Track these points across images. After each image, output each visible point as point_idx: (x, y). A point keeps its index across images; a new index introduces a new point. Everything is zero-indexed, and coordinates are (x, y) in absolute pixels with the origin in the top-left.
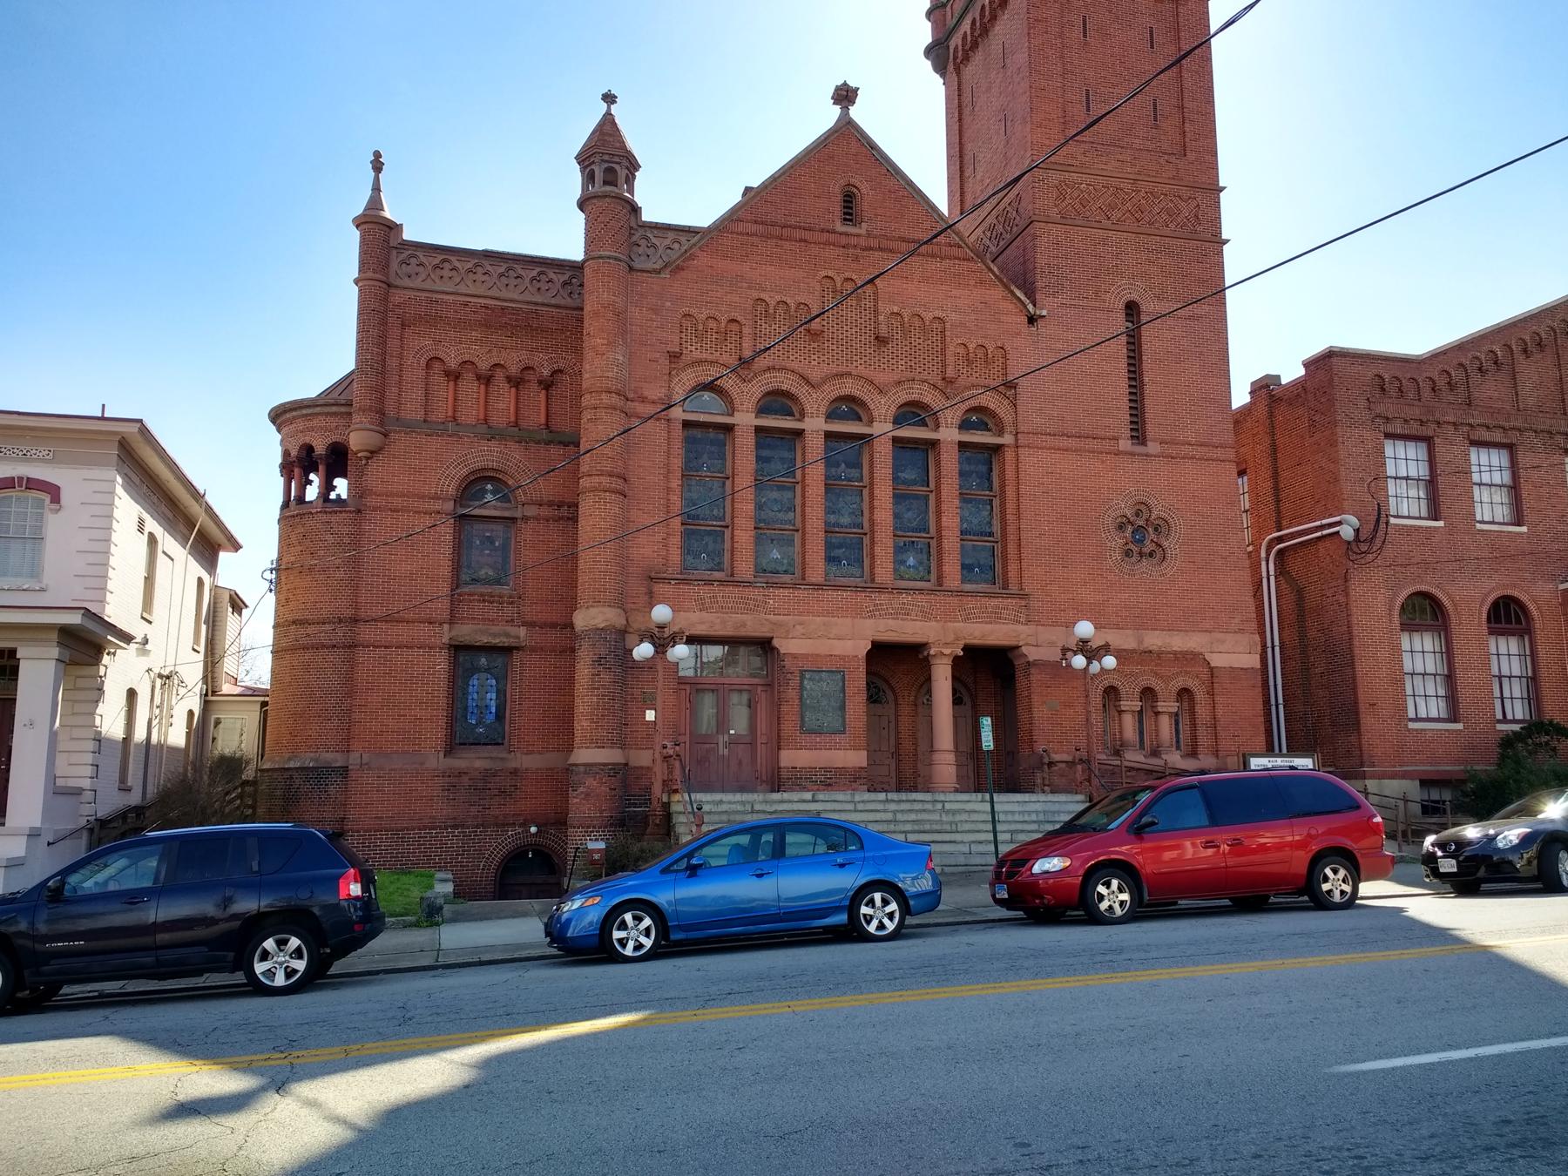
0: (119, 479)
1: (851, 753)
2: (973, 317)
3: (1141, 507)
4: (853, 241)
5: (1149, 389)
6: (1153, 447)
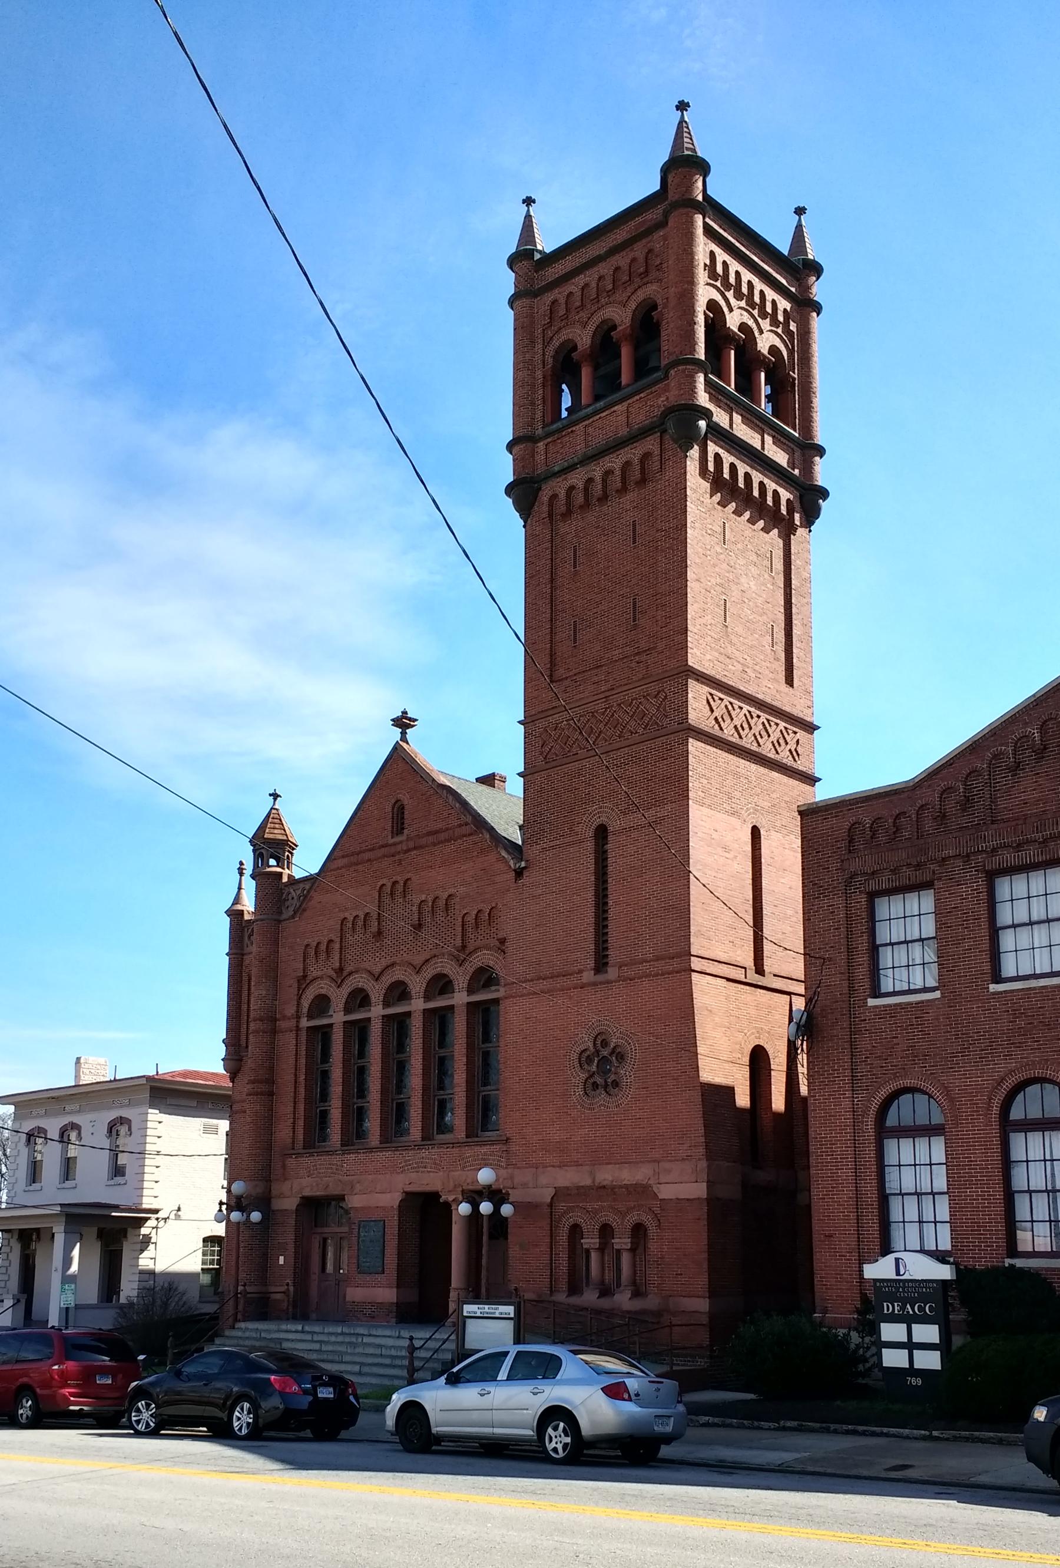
0: (839, 1403)
1: (387, 1290)
2: (475, 885)
3: (601, 1040)
4: (399, 848)
5: (612, 914)
6: (612, 973)
